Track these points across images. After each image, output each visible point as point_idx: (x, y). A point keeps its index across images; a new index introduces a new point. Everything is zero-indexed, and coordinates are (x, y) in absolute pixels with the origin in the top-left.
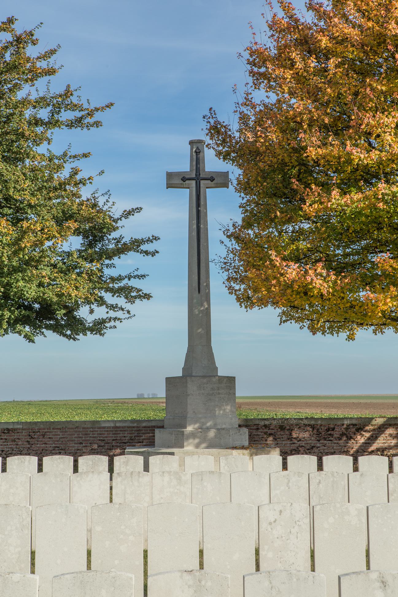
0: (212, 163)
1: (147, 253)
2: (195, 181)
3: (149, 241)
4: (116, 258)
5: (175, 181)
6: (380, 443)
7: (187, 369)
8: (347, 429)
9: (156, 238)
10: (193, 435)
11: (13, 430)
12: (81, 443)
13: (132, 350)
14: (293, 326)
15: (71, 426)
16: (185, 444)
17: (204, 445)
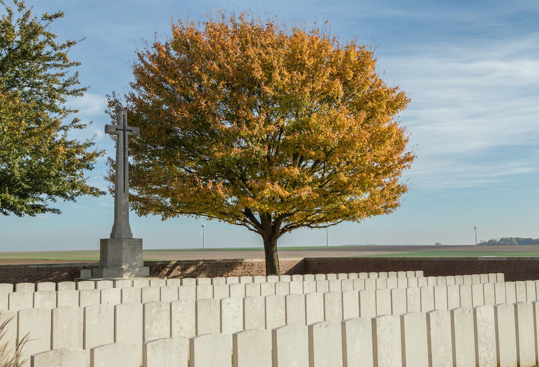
3: (88, 145)
6: (173, 274)
7: (112, 235)
8: (158, 267)
10: (128, 271)
12: (17, 278)
15: (11, 268)
16: (124, 275)
17: (133, 276)
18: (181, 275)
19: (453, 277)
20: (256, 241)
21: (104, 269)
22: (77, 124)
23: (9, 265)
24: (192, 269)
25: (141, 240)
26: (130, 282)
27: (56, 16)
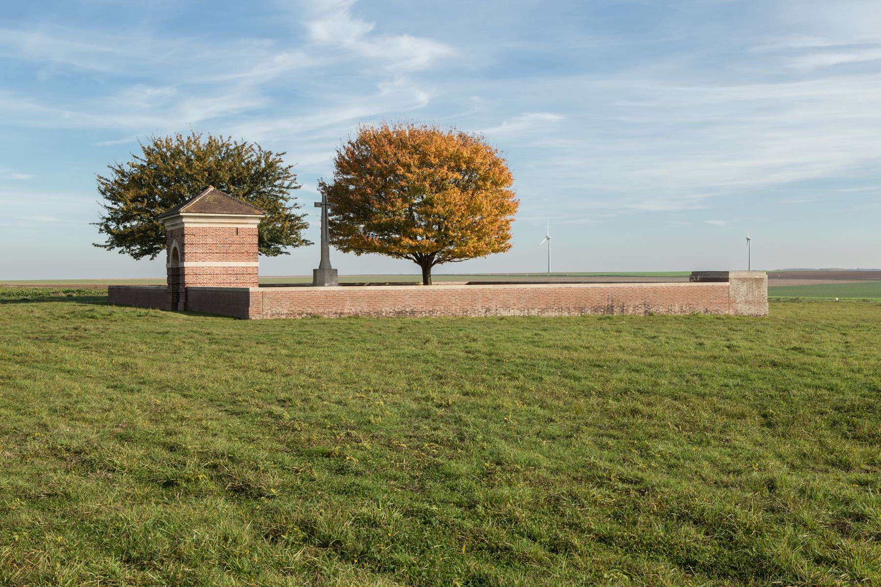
20: (418, 270)
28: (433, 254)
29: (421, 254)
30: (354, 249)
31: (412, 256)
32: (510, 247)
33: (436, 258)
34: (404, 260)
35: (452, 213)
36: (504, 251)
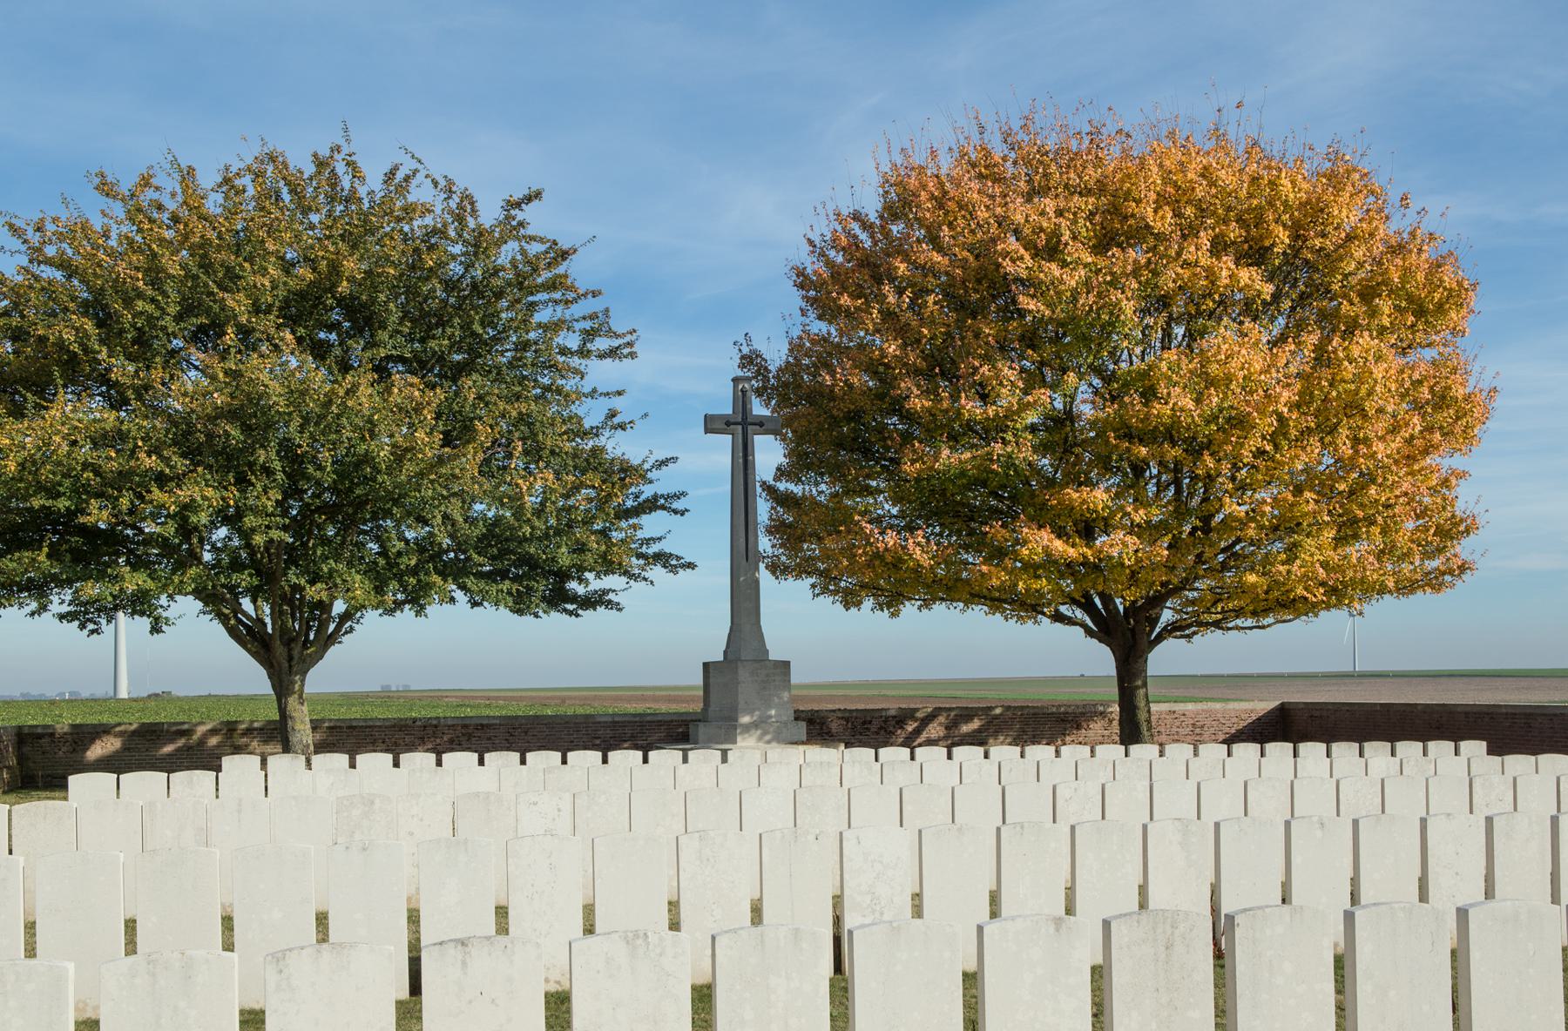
0: (759, 409)
1: (675, 512)
2: (738, 426)
4: (644, 517)
5: (712, 424)
9: (684, 494)
11: (488, 726)
13: (656, 627)
14: (826, 600)
16: (739, 738)
17: (768, 737)
18: (945, 738)
19: (1533, 758)
20: (1099, 660)
21: (701, 725)
22: (616, 420)
23: (536, 717)
24: (975, 724)
25: (787, 664)
26: (758, 755)
27: (529, 199)
28: (1157, 601)
29: (1107, 599)
30: (873, 589)
31: (1079, 614)
32: (1463, 568)
33: (1167, 616)
34: (1046, 627)
35: (1240, 423)
36: (1437, 587)
